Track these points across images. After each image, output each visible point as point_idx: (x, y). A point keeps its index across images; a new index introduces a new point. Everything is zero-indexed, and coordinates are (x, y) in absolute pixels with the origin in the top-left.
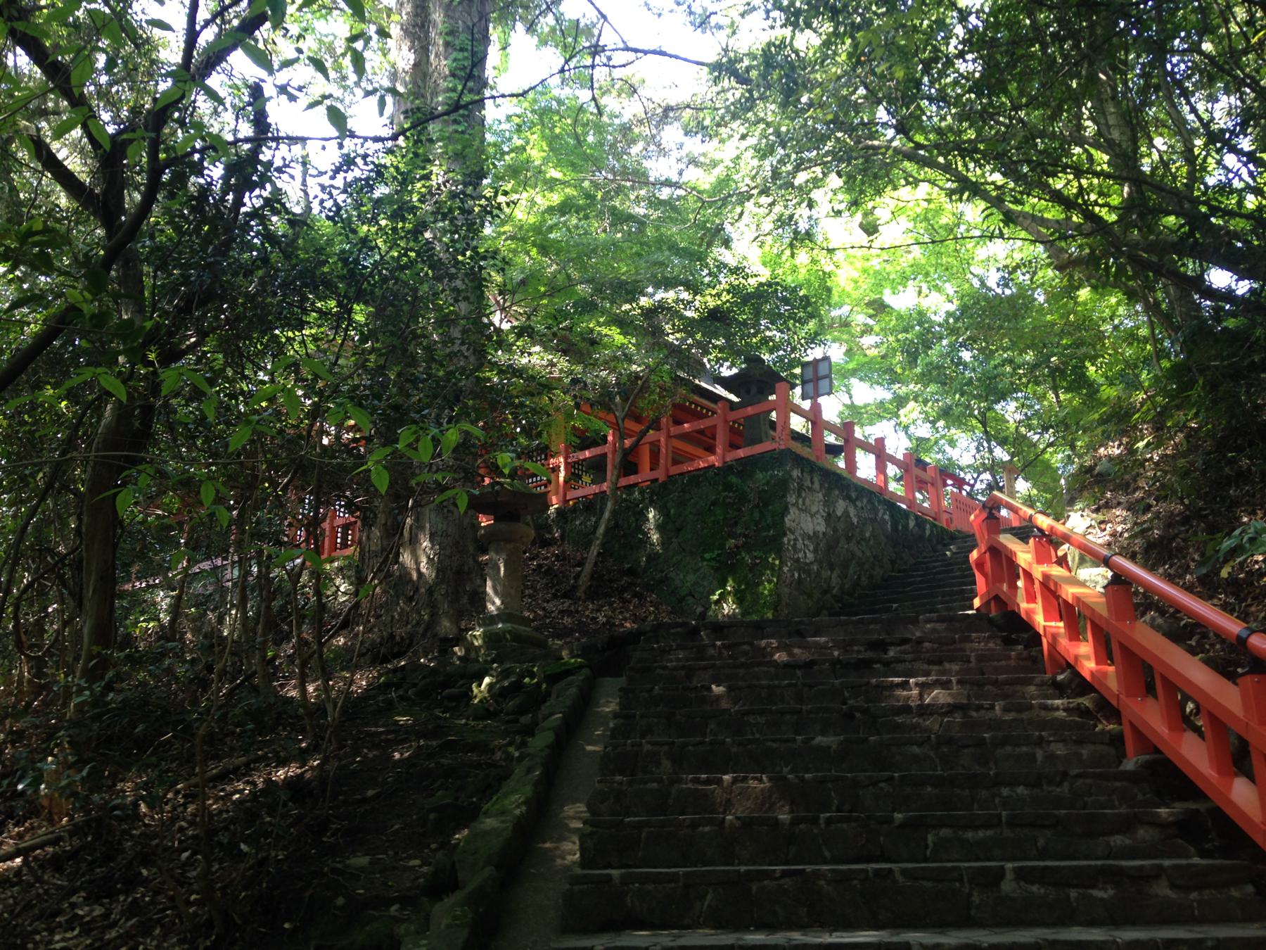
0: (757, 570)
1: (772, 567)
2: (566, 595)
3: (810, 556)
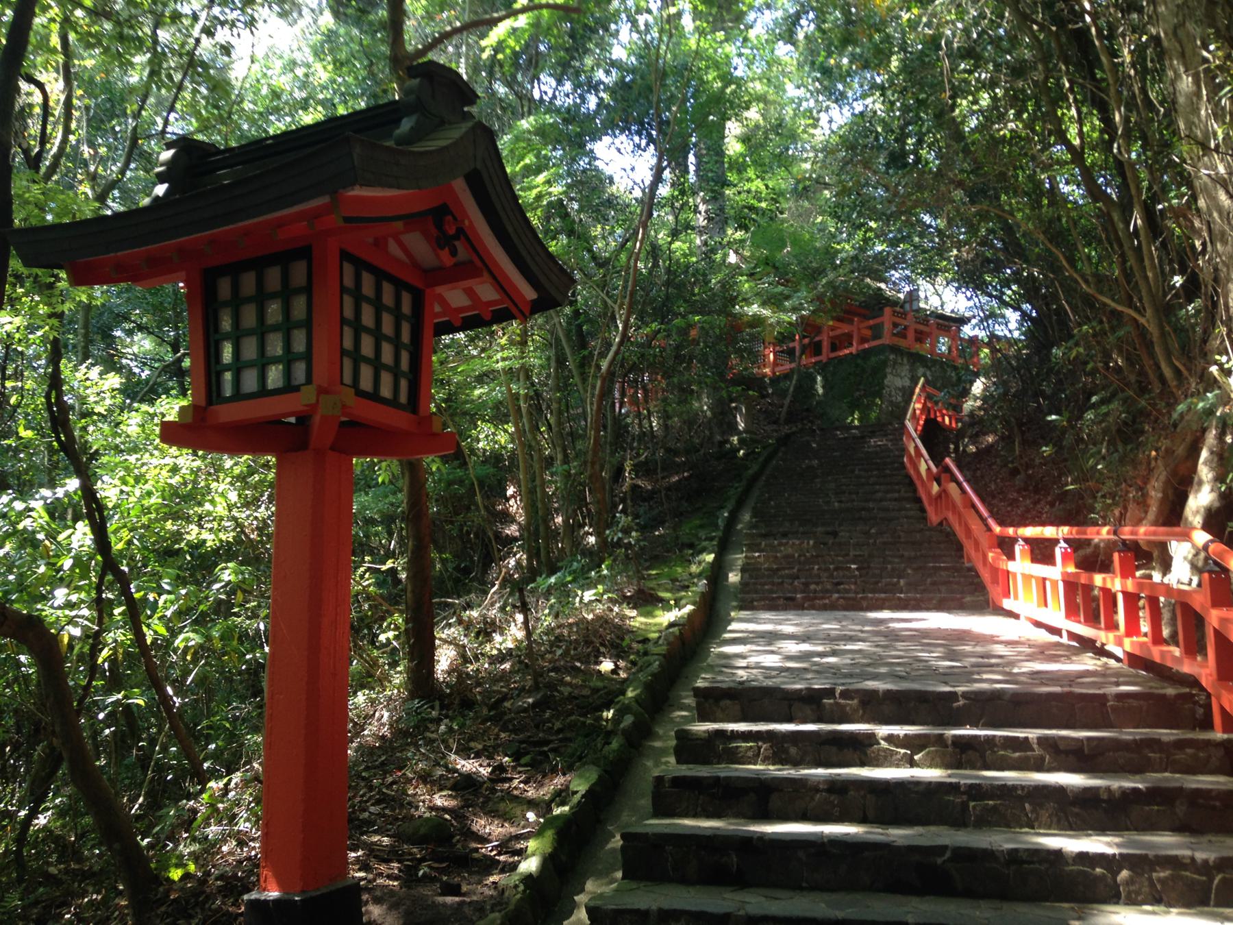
0: (869, 407)
1: (877, 405)
2: (774, 423)
3: (900, 399)
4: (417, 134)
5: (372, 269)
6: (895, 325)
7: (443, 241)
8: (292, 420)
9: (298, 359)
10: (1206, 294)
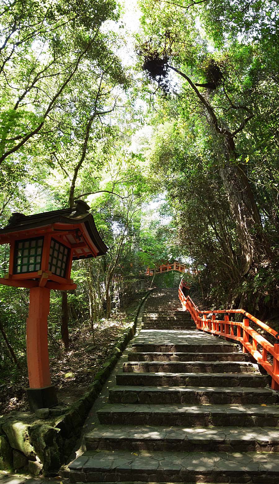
4: (75, 215)
5: (58, 243)
6: (176, 266)
7: (78, 237)
8: (34, 279)
9: (38, 264)
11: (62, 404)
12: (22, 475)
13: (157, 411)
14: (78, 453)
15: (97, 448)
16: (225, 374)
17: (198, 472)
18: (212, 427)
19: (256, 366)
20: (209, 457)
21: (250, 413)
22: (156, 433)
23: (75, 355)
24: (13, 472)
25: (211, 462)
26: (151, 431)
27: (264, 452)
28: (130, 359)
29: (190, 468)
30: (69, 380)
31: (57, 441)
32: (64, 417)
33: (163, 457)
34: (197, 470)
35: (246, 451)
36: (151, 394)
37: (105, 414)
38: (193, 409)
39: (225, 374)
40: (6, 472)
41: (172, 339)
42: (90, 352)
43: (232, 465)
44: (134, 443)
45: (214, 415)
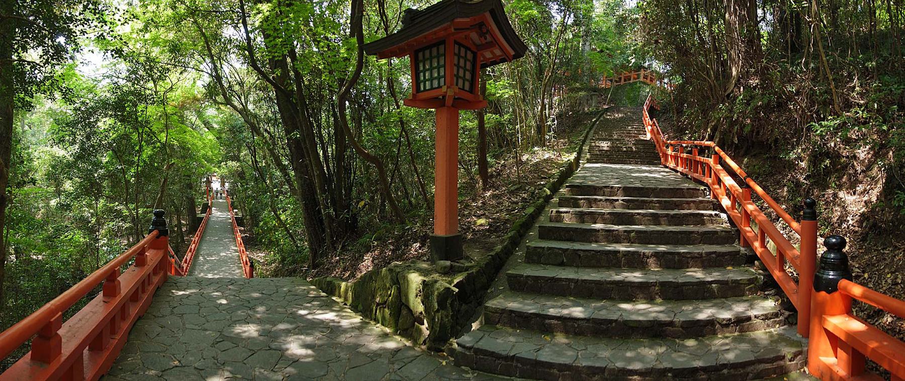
5: (464, 46)
7: (482, 35)
10: (357, 337)
11: (468, 258)
12: (403, 339)
13: (586, 277)
14: (475, 326)
15: (499, 322)
16: (684, 228)
17: (631, 371)
18: (659, 300)
19: (724, 216)
20: (651, 347)
21: (710, 279)
22: (580, 309)
23: (494, 196)
24: (395, 333)
25: (650, 354)
26: (574, 306)
27: (727, 335)
28: (561, 205)
29: (620, 364)
30: (482, 228)
31: (452, 305)
32: (465, 274)
33: (586, 345)
34: (630, 368)
35: (703, 336)
36: (582, 254)
37: (516, 276)
38: (635, 276)
39: (684, 228)
40: (388, 330)
41: (620, 179)
42: (512, 193)
43: (680, 360)
44: (547, 321)
45: (663, 284)
